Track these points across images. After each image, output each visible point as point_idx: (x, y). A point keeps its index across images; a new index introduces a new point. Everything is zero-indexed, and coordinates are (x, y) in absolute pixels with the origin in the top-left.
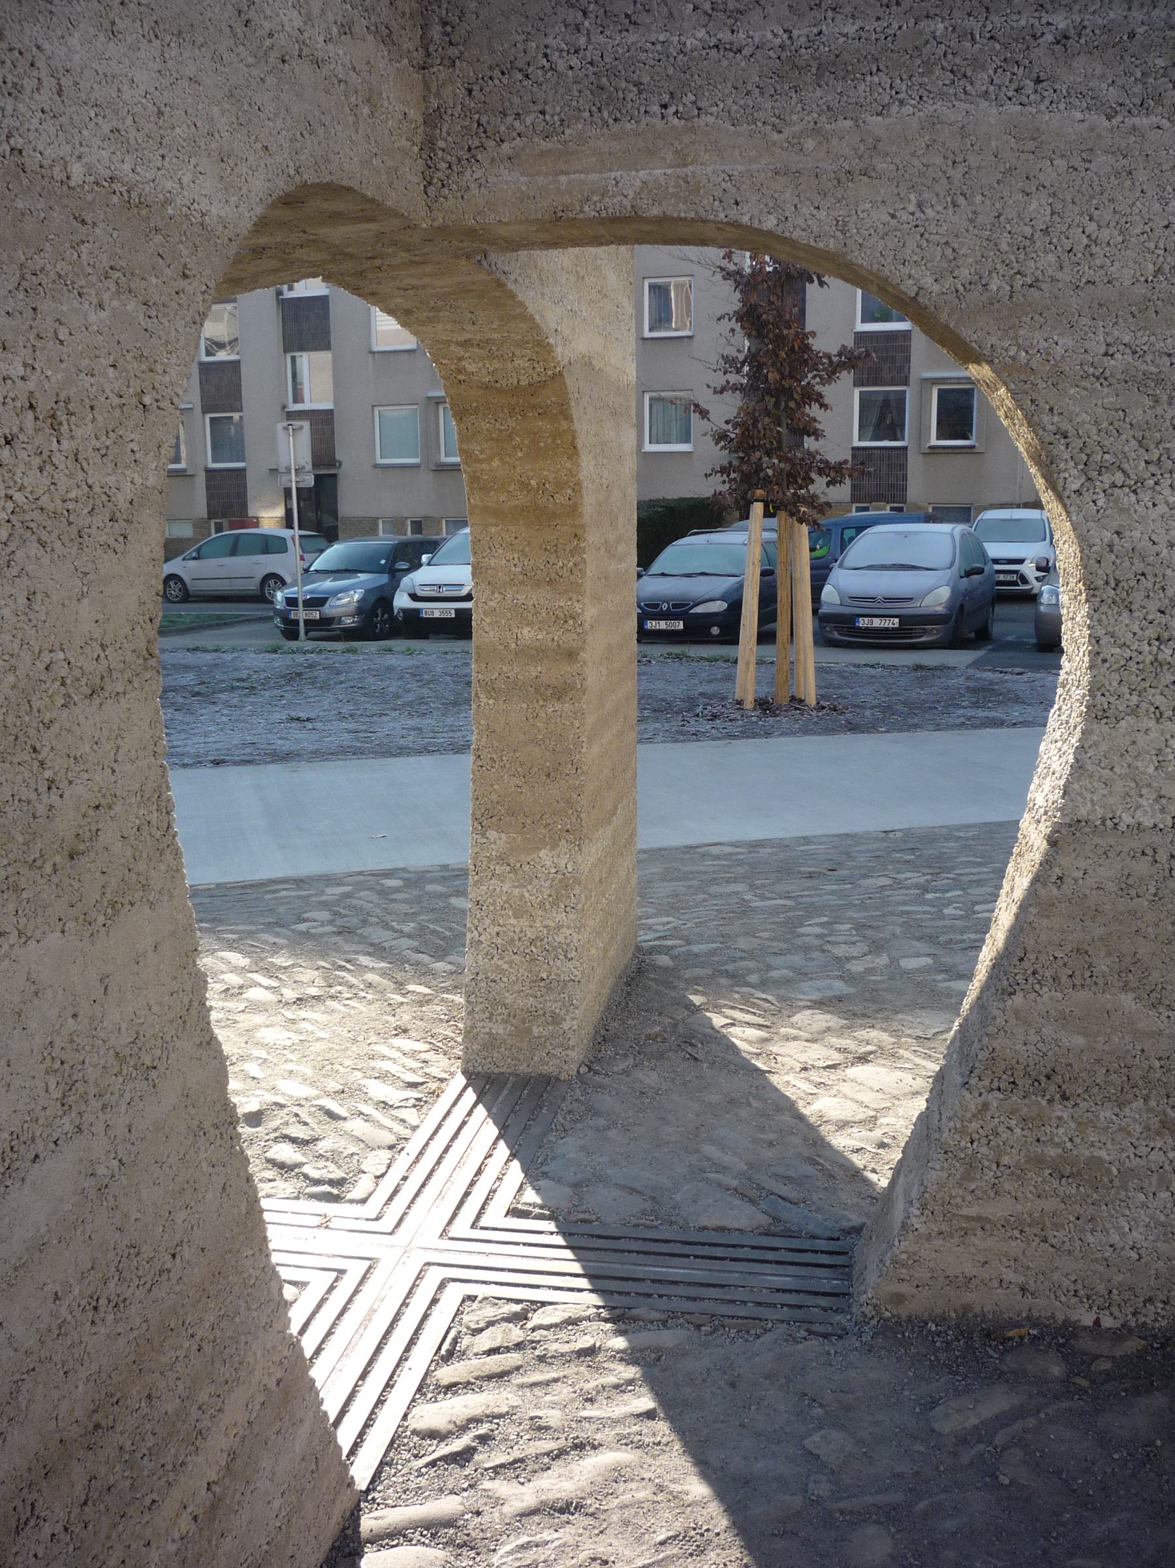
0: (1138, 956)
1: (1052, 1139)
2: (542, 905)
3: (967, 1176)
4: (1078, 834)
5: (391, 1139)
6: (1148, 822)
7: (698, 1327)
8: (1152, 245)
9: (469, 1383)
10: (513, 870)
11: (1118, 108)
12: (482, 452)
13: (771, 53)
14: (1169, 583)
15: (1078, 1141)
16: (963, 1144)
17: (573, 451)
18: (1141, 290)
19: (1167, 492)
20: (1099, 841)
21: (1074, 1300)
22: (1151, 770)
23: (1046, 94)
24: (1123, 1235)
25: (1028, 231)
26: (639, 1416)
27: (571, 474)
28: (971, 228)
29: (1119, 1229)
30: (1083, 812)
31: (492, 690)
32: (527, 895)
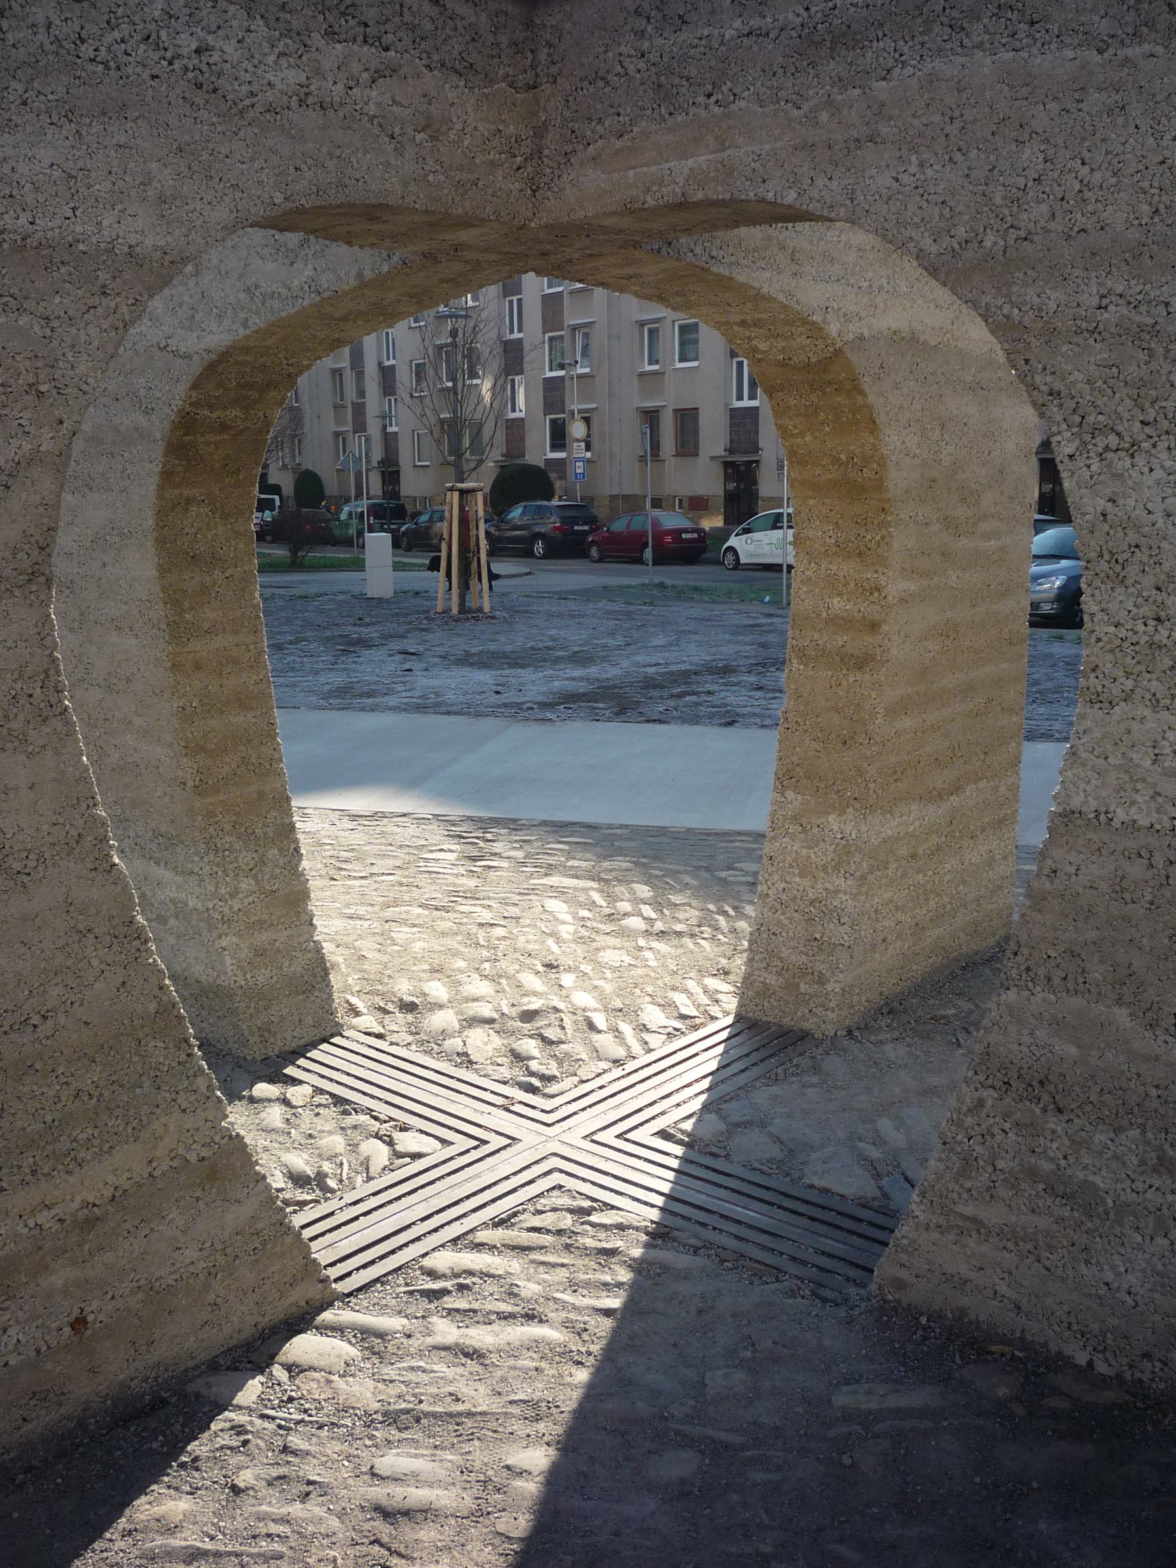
0: (1133, 969)
1: (1045, 1152)
2: (824, 869)
3: (963, 1173)
4: (1071, 826)
5: (621, 1053)
6: (1144, 822)
7: (723, 1261)
8: (1146, 184)
9: (495, 1247)
10: (804, 830)
11: (1110, 41)
12: (795, 427)
13: (793, 33)
14: (1165, 557)
15: (1072, 1160)
16: (959, 1138)
17: (873, 426)
18: (1135, 234)
19: (1164, 455)
20: (1091, 835)
21: (1067, 1333)
22: (1147, 763)
23: (1038, 36)
24: (1118, 1274)
25: (1021, 181)
26: (597, 1310)
27: (875, 448)
28: (966, 184)
29: (1113, 1267)
30: (1076, 802)
31: (802, 656)
32: (813, 856)
